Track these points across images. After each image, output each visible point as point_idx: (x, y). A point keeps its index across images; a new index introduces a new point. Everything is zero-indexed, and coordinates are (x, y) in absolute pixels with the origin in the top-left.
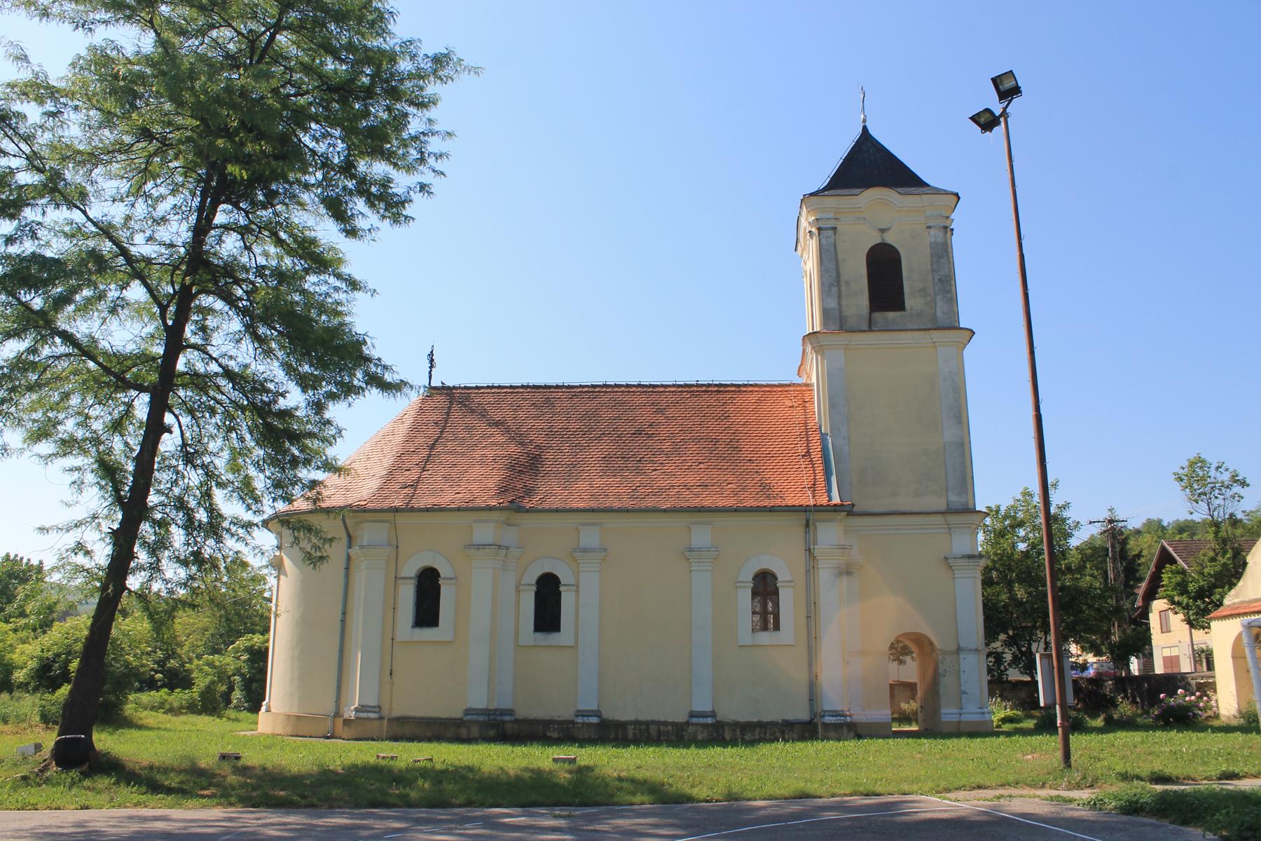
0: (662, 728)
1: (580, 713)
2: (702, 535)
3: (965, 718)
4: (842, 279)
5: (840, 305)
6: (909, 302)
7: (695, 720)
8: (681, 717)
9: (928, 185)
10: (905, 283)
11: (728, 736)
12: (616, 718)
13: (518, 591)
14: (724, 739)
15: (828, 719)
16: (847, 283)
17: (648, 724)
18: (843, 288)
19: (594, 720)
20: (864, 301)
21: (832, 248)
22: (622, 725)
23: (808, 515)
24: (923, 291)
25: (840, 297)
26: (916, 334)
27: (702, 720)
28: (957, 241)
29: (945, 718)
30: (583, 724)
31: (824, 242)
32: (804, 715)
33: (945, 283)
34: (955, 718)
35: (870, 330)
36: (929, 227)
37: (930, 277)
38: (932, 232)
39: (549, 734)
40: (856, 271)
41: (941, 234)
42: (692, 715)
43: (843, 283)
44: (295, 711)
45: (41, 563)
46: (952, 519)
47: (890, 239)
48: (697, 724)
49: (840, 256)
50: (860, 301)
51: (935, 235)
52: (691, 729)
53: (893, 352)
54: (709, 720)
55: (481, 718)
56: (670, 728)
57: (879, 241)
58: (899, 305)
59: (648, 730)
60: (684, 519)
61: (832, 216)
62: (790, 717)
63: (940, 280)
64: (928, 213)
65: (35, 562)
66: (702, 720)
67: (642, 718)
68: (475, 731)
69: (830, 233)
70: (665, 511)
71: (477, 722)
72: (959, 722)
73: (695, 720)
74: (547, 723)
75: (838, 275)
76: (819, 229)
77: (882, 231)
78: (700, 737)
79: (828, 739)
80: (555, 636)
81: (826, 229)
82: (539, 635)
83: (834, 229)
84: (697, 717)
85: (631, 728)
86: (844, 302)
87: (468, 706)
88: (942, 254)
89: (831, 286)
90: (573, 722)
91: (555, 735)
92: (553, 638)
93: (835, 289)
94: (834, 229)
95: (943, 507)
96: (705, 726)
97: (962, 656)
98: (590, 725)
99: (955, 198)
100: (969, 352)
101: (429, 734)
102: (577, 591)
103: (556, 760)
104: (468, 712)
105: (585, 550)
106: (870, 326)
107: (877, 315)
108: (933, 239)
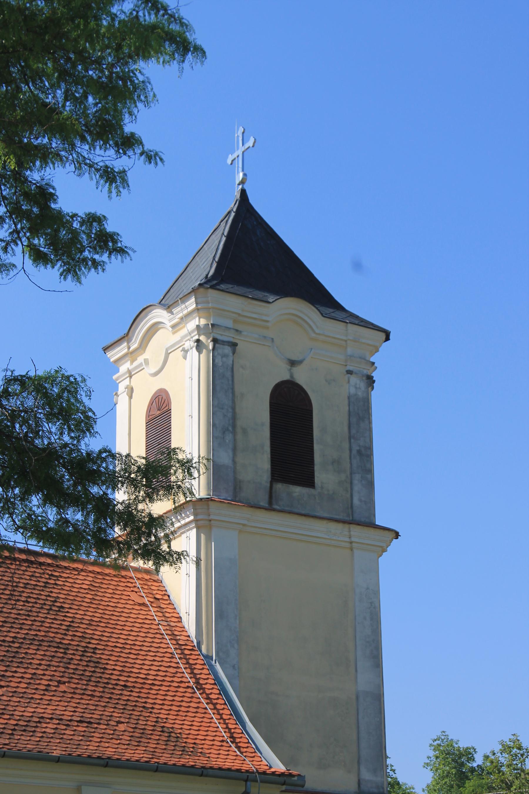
4: (239, 423)
5: (234, 462)
6: (321, 476)
9: (338, 307)
10: (317, 447)
16: (245, 431)
18: (239, 436)
20: (263, 462)
21: (228, 374)
24: (336, 462)
26: (333, 526)
28: (377, 397)
31: (218, 361)
33: (362, 457)
35: (270, 508)
36: (350, 372)
37: (346, 445)
38: (354, 379)
40: (257, 413)
41: (362, 385)
43: (239, 430)
45: (164, 66)
47: (301, 377)
49: (238, 389)
50: (258, 464)
53: (293, 545)
57: (286, 377)
58: (307, 480)
61: (229, 323)
63: (359, 452)
64: (349, 351)
65: (139, 122)
69: (227, 350)
70: (58, 760)
75: (234, 418)
76: (215, 341)
77: (293, 363)
81: (224, 343)
83: (234, 345)
88: (360, 413)
89: (225, 431)
93: (229, 437)
94: (234, 345)
99: (383, 336)
100: (384, 561)
106: (270, 503)
107: (279, 486)
108: (353, 391)
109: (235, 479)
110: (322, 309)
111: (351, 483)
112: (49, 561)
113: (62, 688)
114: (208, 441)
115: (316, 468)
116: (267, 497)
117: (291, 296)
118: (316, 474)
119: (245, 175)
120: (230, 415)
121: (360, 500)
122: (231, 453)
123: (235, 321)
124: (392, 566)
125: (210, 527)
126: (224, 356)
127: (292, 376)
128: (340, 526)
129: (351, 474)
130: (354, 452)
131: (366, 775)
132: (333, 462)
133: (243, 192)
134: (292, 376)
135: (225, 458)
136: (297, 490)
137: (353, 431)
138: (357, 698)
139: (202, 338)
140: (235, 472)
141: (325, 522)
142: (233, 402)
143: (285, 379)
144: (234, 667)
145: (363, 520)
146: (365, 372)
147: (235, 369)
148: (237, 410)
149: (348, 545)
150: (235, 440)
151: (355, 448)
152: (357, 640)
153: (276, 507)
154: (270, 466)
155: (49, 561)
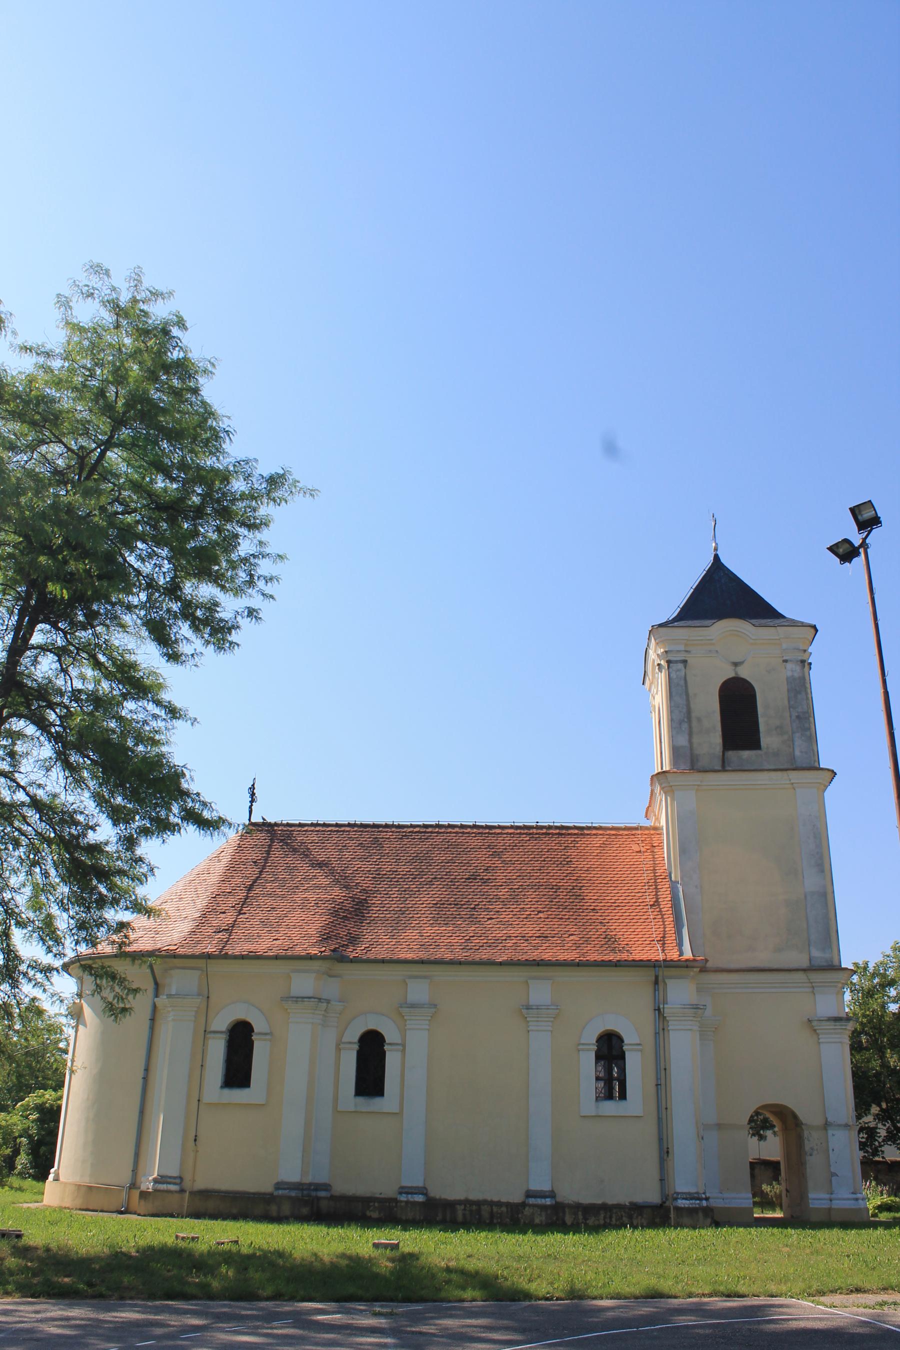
0: (495, 1209)
1: (404, 1190)
2: (541, 991)
3: (836, 1204)
4: (693, 715)
6: (765, 740)
7: (532, 1201)
8: (517, 1198)
9: (780, 616)
10: (761, 720)
11: (569, 1220)
12: (444, 1196)
13: (338, 1049)
14: (564, 1223)
15: (681, 1203)
16: (699, 720)
17: (479, 1203)
18: (694, 723)
19: (420, 1198)
20: (716, 739)
21: (682, 682)
22: (450, 1205)
23: (658, 972)
25: (690, 734)
27: (540, 1201)
28: (817, 678)
29: (813, 1204)
30: (407, 1202)
31: (673, 675)
32: (652, 1196)
33: (803, 720)
34: (825, 1205)
35: (724, 769)
36: (785, 661)
37: (788, 714)
38: (789, 666)
39: (368, 1213)
40: (709, 706)
41: (798, 668)
42: (529, 1194)
44: (86, 1181)
46: (816, 977)
47: (744, 673)
48: (534, 1206)
50: (712, 739)
51: (793, 669)
52: (527, 1211)
53: (747, 794)
54: (548, 1202)
55: (293, 1194)
56: (504, 1209)
58: (754, 743)
59: (479, 1211)
60: (517, 975)
61: (682, 648)
62: (639, 1199)
63: (798, 717)
64: (784, 646)
66: (540, 1201)
67: (474, 1196)
68: (286, 1209)
70: (501, 964)
71: (290, 1198)
72: (830, 1209)
73: (532, 1201)
74: (367, 1201)
77: (736, 664)
78: (537, 1221)
79: (682, 1226)
80: (377, 1100)
81: (676, 662)
82: (361, 1100)
83: (685, 662)
84: (535, 1197)
85: (460, 1208)
86: (695, 740)
87: (279, 1180)
88: (800, 689)
89: (681, 722)
90: (395, 1200)
91: (375, 1215)
92: (376, 1103)
93: (685, 726)
94: (685, 662)
95: (805, 964)
96: (543, 1208)
97: (830, 1132)
98: (415, 1203)
99: (813, 631)
101: (235, 1211)
102: (403, 1051)
103: (376, 1246)
104: (279, 1186)
105: (413, 1006)
107: (731, 754)
108: (789, 674)
109: (692, 754)
110: (753, 621)
111: (793, 741)
112: (576, 831)
113: (541, 915)
114: (669, 732)
115: (761, 735)
116: (720, 763)
117: (726, 618)
118: (762, 739)
119: (717, 544)
120: (685, 710)
121: (801, 752)
122: (687, 737)
123: (686, 645)
124: (833, 795)
125: (673, 791)
126: (678, 670)
127: (736, 673)
128: (779, 773)
129: (793, 733)
130: (794, 717)
131: (816, 953)
132: (777, 728)
133: (716, 558)
134: (736, 673)
135: (683, 741)
136: (746, 754)
137: (792, 703)
138: (806, 897)
139: (662, 662)
140: (691, 748)
141: (766, 773)
142: (688, 700)
143: (731, 677)
144: (696, 887)
145: (804, 766)
146: (800, 658)
147: (688, 679)
148: (692, 706)
149: (790, 786)
150: (690, 727)
151: (794, 714)
152: (808, 857)
153: (727, 768)
154: (721, 741)
155: (576, 831)
